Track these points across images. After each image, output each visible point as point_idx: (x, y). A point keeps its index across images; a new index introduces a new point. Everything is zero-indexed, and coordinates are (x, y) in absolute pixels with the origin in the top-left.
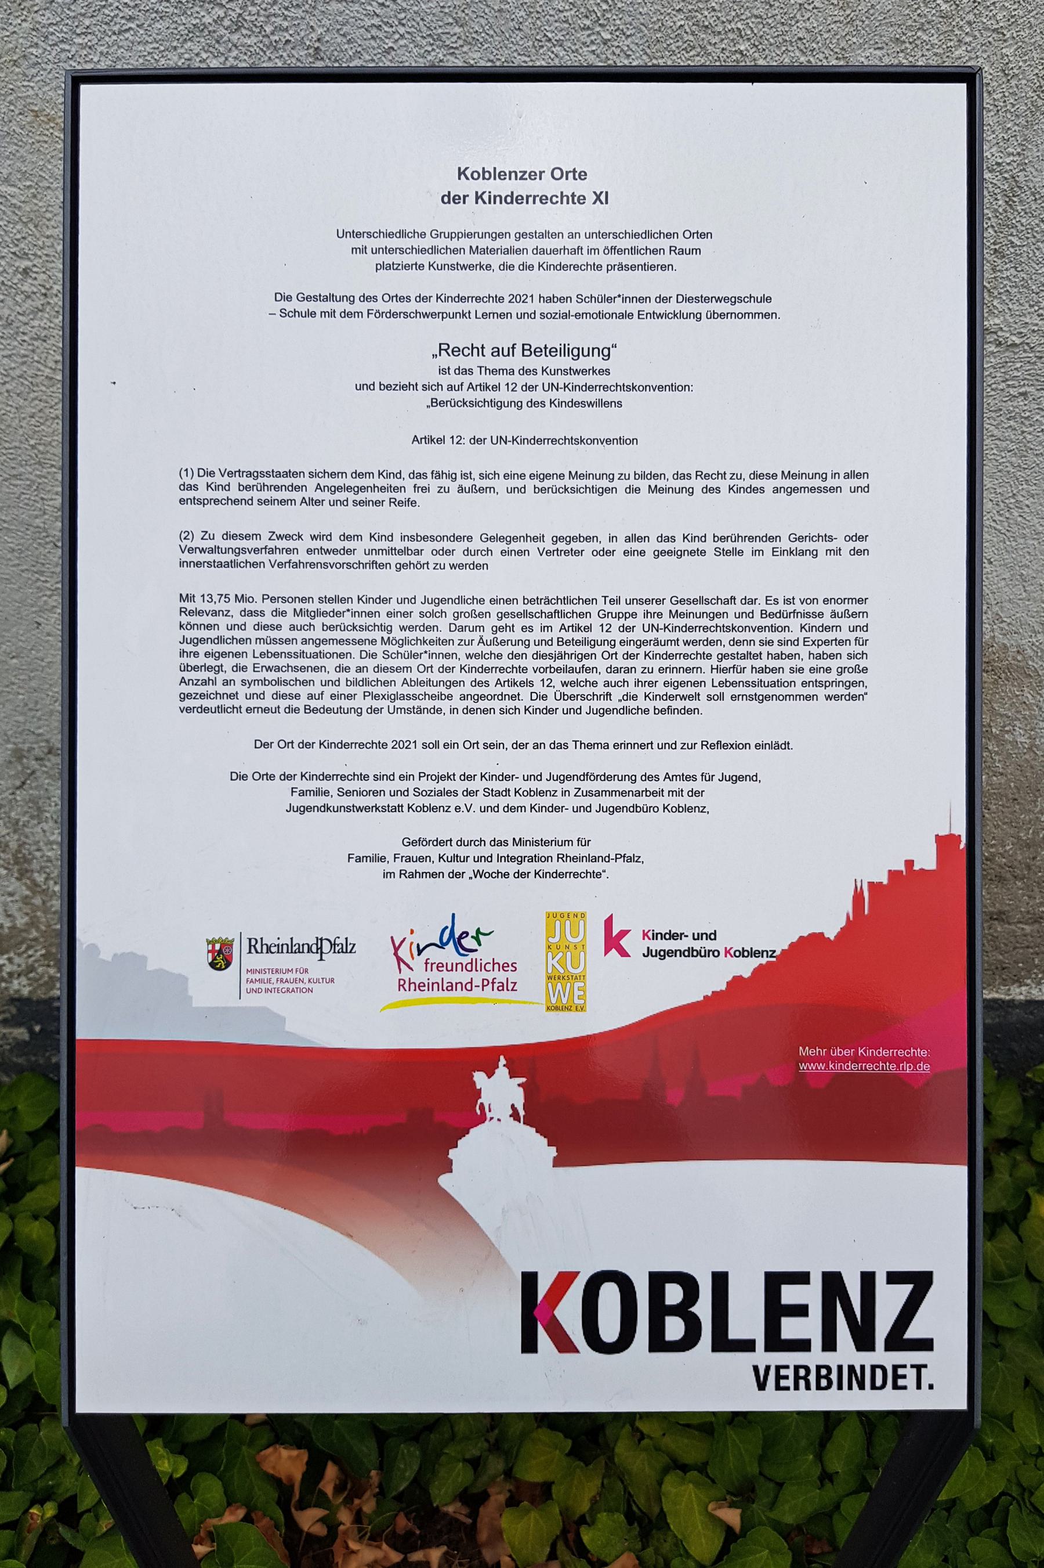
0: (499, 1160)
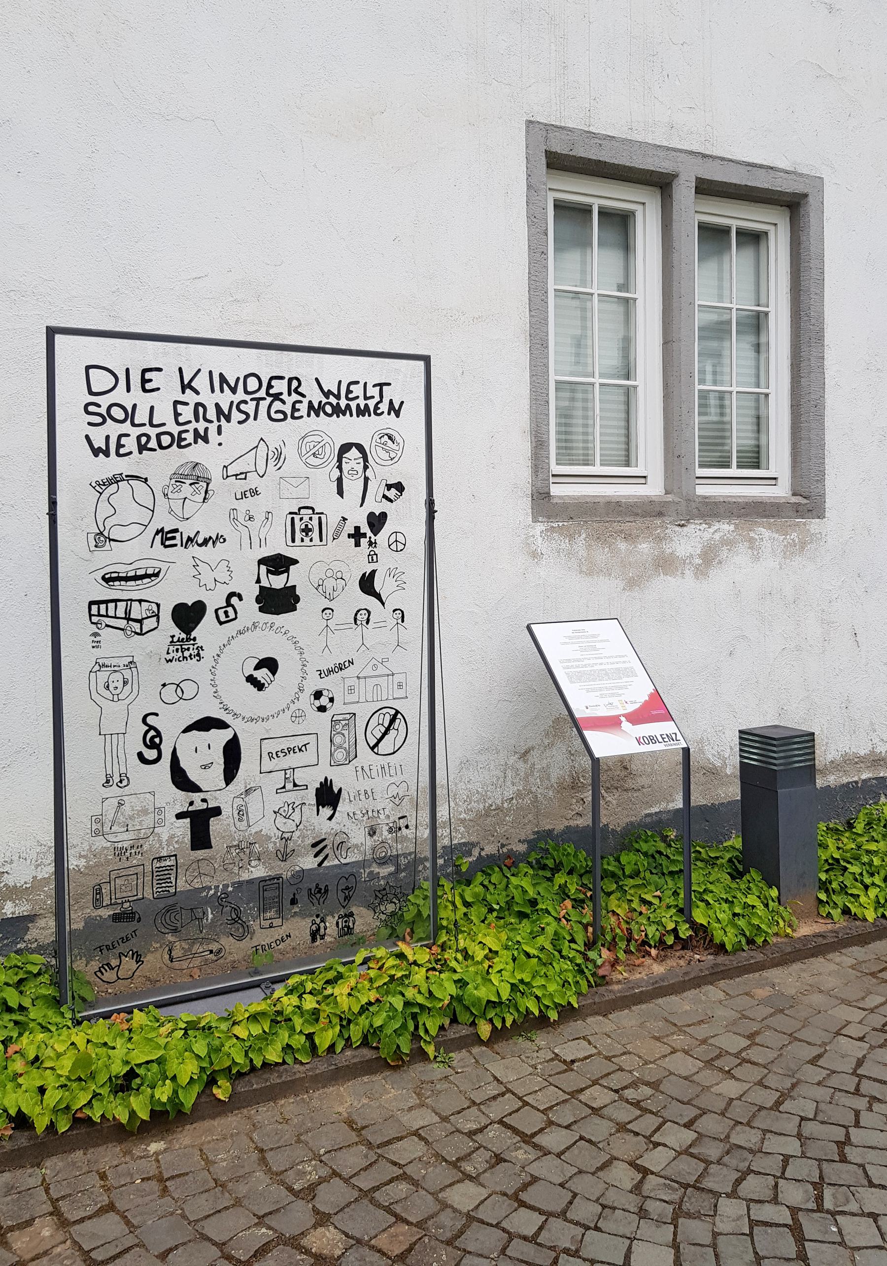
0: (626, 725)
